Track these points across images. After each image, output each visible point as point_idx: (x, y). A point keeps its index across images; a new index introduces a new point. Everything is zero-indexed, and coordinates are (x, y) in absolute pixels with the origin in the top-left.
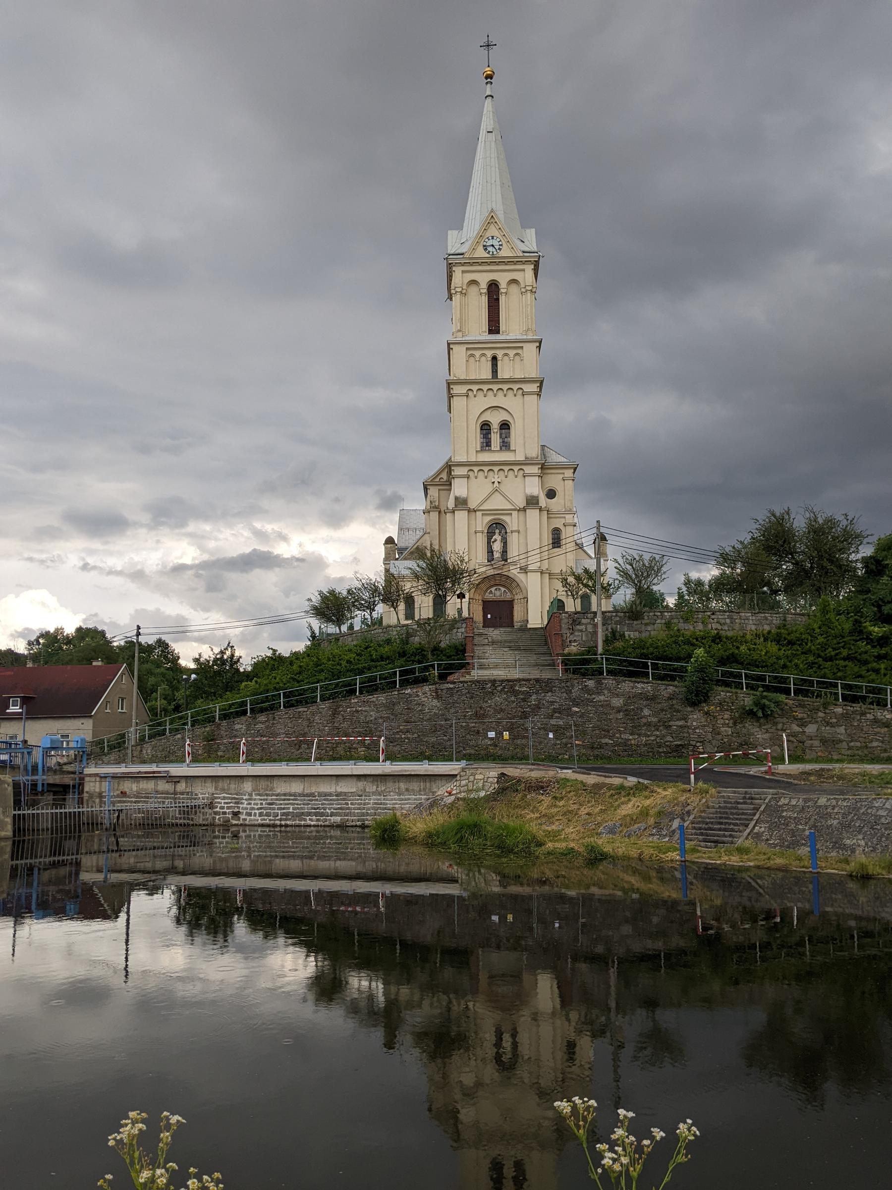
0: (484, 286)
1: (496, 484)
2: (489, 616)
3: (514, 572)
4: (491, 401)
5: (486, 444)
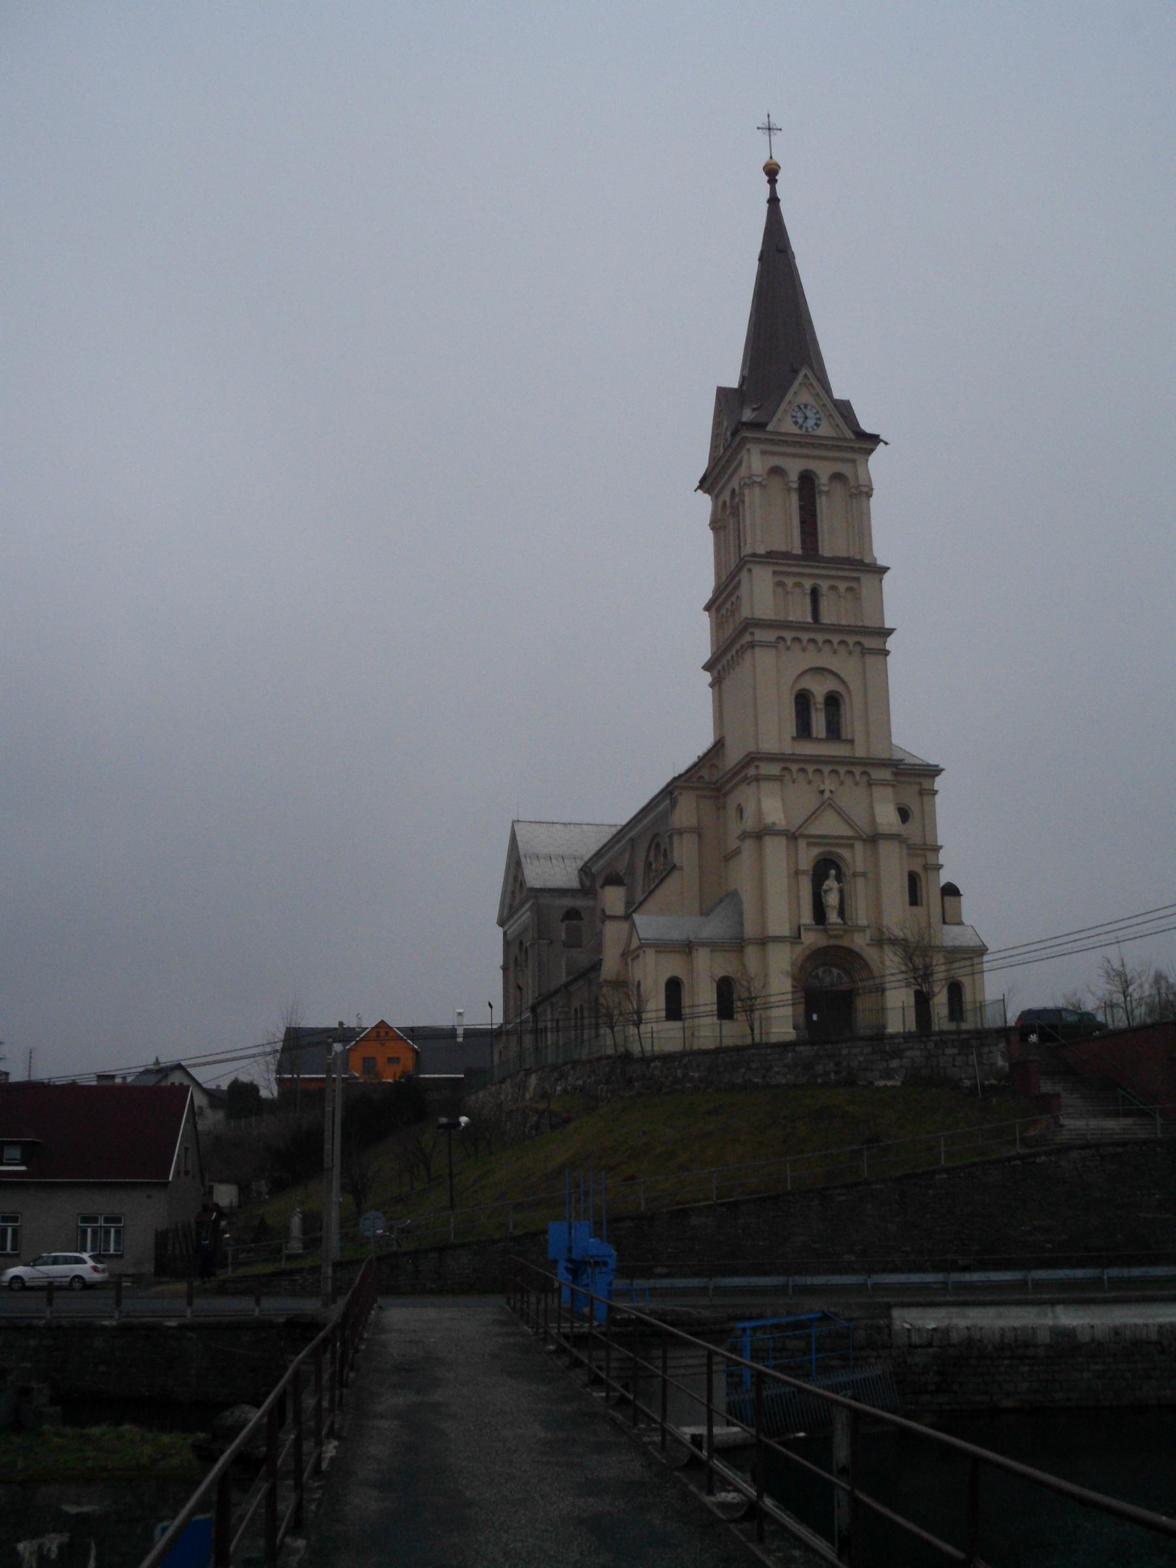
0: (794, 477)
2: (815, 1017)
3: (860, 942)
4: (812, 659)
5: (804, 730)
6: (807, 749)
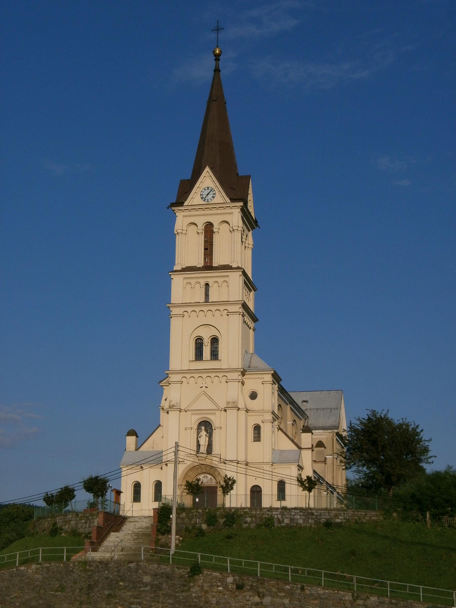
0: (201, 227)
1: (204, 387)
5: (199, 356)
6: (199, 365)
